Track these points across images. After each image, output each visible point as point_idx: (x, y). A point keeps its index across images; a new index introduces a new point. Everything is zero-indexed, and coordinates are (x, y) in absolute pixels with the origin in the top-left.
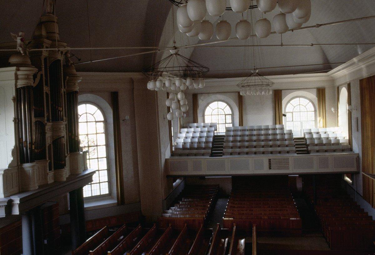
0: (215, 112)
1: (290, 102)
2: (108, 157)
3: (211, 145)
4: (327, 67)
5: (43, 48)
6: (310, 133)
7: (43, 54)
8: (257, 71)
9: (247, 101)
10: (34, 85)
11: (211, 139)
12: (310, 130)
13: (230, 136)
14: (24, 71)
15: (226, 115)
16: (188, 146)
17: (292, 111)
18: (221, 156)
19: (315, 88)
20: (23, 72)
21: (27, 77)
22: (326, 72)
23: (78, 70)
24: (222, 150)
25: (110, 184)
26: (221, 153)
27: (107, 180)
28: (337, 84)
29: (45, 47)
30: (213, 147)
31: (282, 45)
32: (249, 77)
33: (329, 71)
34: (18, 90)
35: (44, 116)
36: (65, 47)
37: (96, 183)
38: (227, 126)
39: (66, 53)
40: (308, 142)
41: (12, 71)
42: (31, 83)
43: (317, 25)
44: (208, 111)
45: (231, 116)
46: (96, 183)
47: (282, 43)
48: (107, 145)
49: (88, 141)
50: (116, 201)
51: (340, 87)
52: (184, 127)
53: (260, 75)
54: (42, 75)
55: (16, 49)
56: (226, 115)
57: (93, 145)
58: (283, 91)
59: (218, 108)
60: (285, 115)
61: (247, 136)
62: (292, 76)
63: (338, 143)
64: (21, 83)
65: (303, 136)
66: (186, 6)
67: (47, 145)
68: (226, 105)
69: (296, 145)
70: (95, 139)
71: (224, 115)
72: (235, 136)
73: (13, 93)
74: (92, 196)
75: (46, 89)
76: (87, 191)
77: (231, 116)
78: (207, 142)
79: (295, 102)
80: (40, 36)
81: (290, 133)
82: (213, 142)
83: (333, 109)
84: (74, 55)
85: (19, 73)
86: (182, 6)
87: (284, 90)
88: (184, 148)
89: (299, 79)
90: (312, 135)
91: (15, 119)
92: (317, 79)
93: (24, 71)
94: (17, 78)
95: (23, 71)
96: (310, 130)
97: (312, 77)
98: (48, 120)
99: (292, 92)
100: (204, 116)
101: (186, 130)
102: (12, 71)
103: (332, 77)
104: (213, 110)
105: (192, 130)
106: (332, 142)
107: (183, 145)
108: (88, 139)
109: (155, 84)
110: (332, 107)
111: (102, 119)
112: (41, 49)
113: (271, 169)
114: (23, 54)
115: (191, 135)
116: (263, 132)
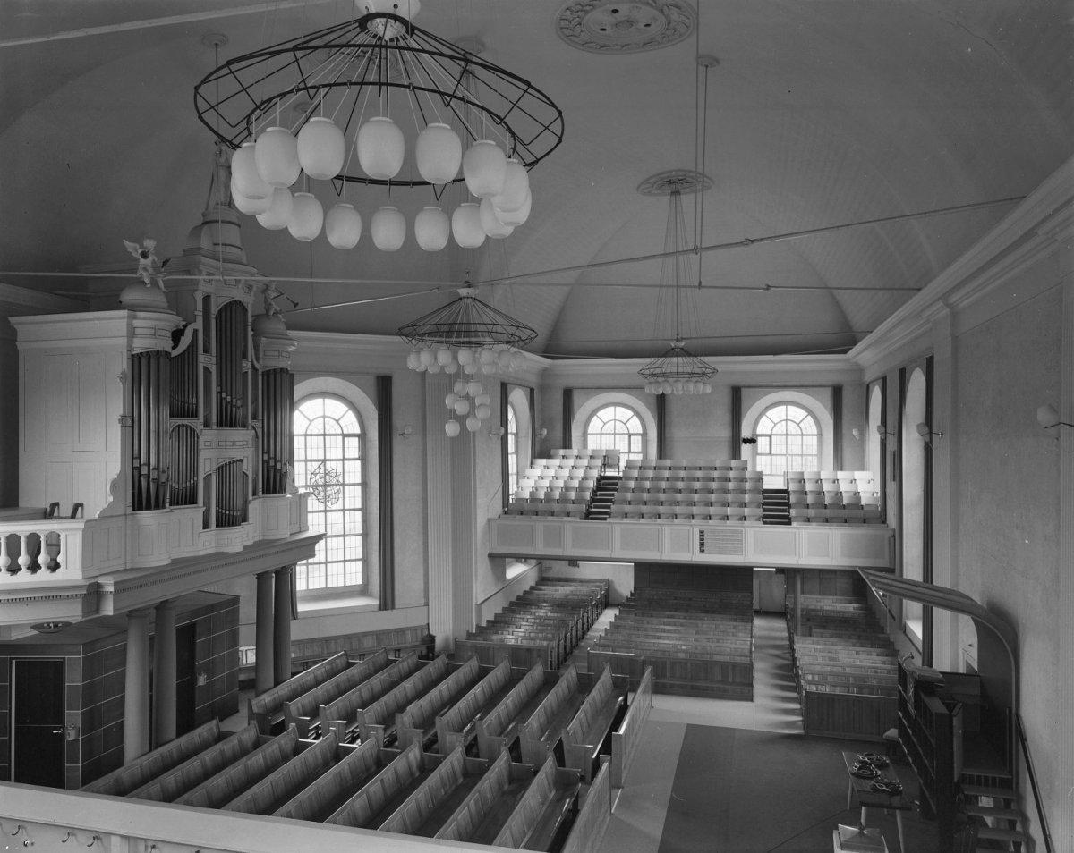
0: (609, 428)
1: (768, 414)
2: (364, 510)
3: (588, 495)
4: (844, 341)
5: (200, 272)
6: (802, 481)
7: (201, 287)
8: (683, 344)
9: (674, 409)
10: (175, 353)
11: (591, 484)
12: (802, 473)
13: (631, 478)
14: (150, 319)
15: (630, 435)
16: (557, 495)
17: (769, 433)
18: (605, 519)
19: (829, 386)
20: (144, 321)
21: (156, 333)
22: (845, 352)
23: (290, 327)
24: (609, 507)
25: (367, 565)
26: (606, 513)
27: (361, 557)
28: (868, 378)
29: (204, 273)
30: (593, 500)
31: (700, 286)
32: (663, 359)
33: (850, 349)
34: (135, 360)
35: (194, 414)
36: (253, 276)
37: (338, 562)
38: (633, 457)
39: (267, 288)
40: (793, 499)
41: (121, 318)
42: (165, 344)
43: (747, 240)
44: (595, 425)
45: (640, 437)
46: (338, 562)
47: (700, 282)
48: (364, 484)
49: (326, 474)
50: (378, 602)
51: (871, 386)
52: (541, 456)
53: (689, 355)
54: (196, 331)
55: (136, 273)
56: (630, 435)
57: (334, 482)
58: (743, 390)
59: (324, 416)
60: (752, 441)
61: (683, 479)
62: (771, 357)
63: (856, 504)
64: (141, 345)
65: (782, 487)
66: (253, 147)
67: (201, 476)
68: (319, 401)
69: (766, 504)
70: (340, 470)
71: (627, 436)
72: (640, 479)
73: (123, 365)
74: (345, 587)
75: (206, 361)
76: (307, 578)
77: (357, 439)
78: (581, 489)
79: (776, 413)
80: (197, 251)
81: (759, 478)
82: (598, 488)
83: (855, 433)
84: (282, 294)
85: (136, 323)
86: (245, 147)
87: (749, 387)
88: (533, 498)
89: (761, 365)
90: (821, 486)
91: (123, 417)
92: (826, 366)
93: (150, 319)
94: (132, 334)
95: (144, 319)
96: (802, 473)
97: (760, 362)
98: (207, 424)
99: (770, 393)
100: (585, 434)
101: (543, 462)
102: (121, 318)
103: (857, 364)
104: (311, 422)
105: (556, 462)
106: (845, 502)
107: (546, 494)
108: (325, 469)
109: (419, 360)
110: (855, 427)
111: (357, 430)
112: (196, 277)
113: (703, 551)
114: (149, 286)
115: (552, 472)
116: (716, 474)
